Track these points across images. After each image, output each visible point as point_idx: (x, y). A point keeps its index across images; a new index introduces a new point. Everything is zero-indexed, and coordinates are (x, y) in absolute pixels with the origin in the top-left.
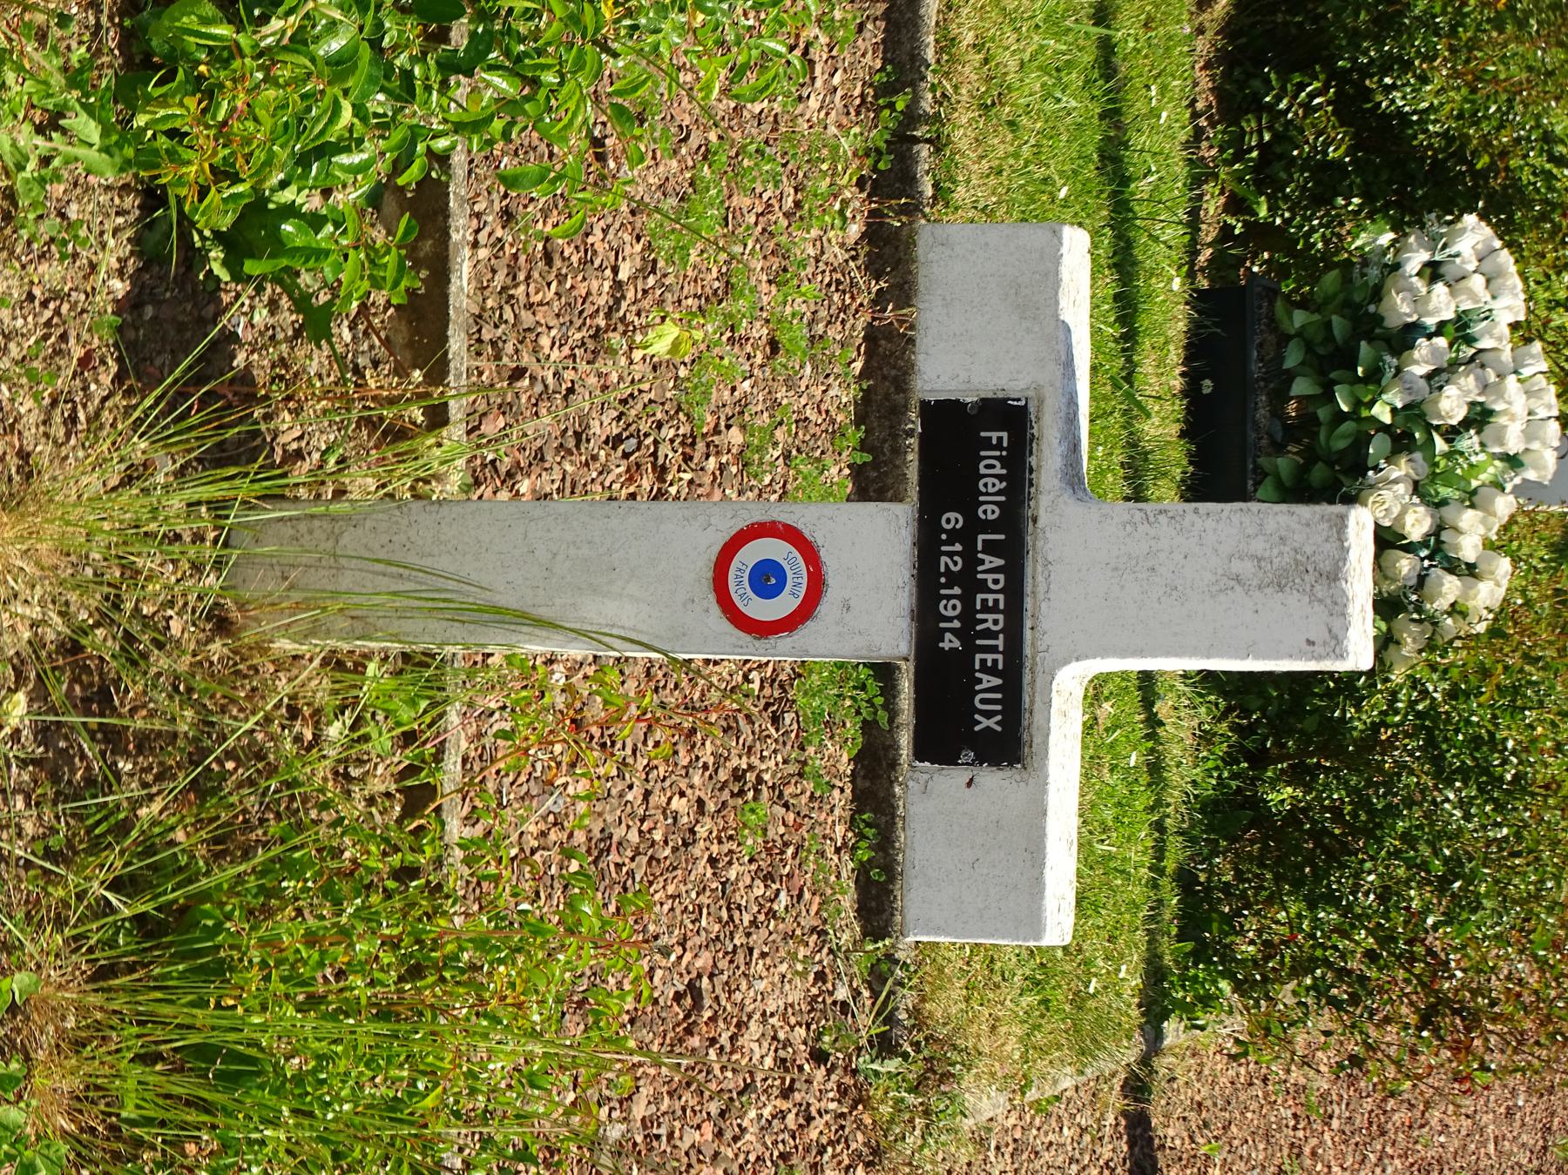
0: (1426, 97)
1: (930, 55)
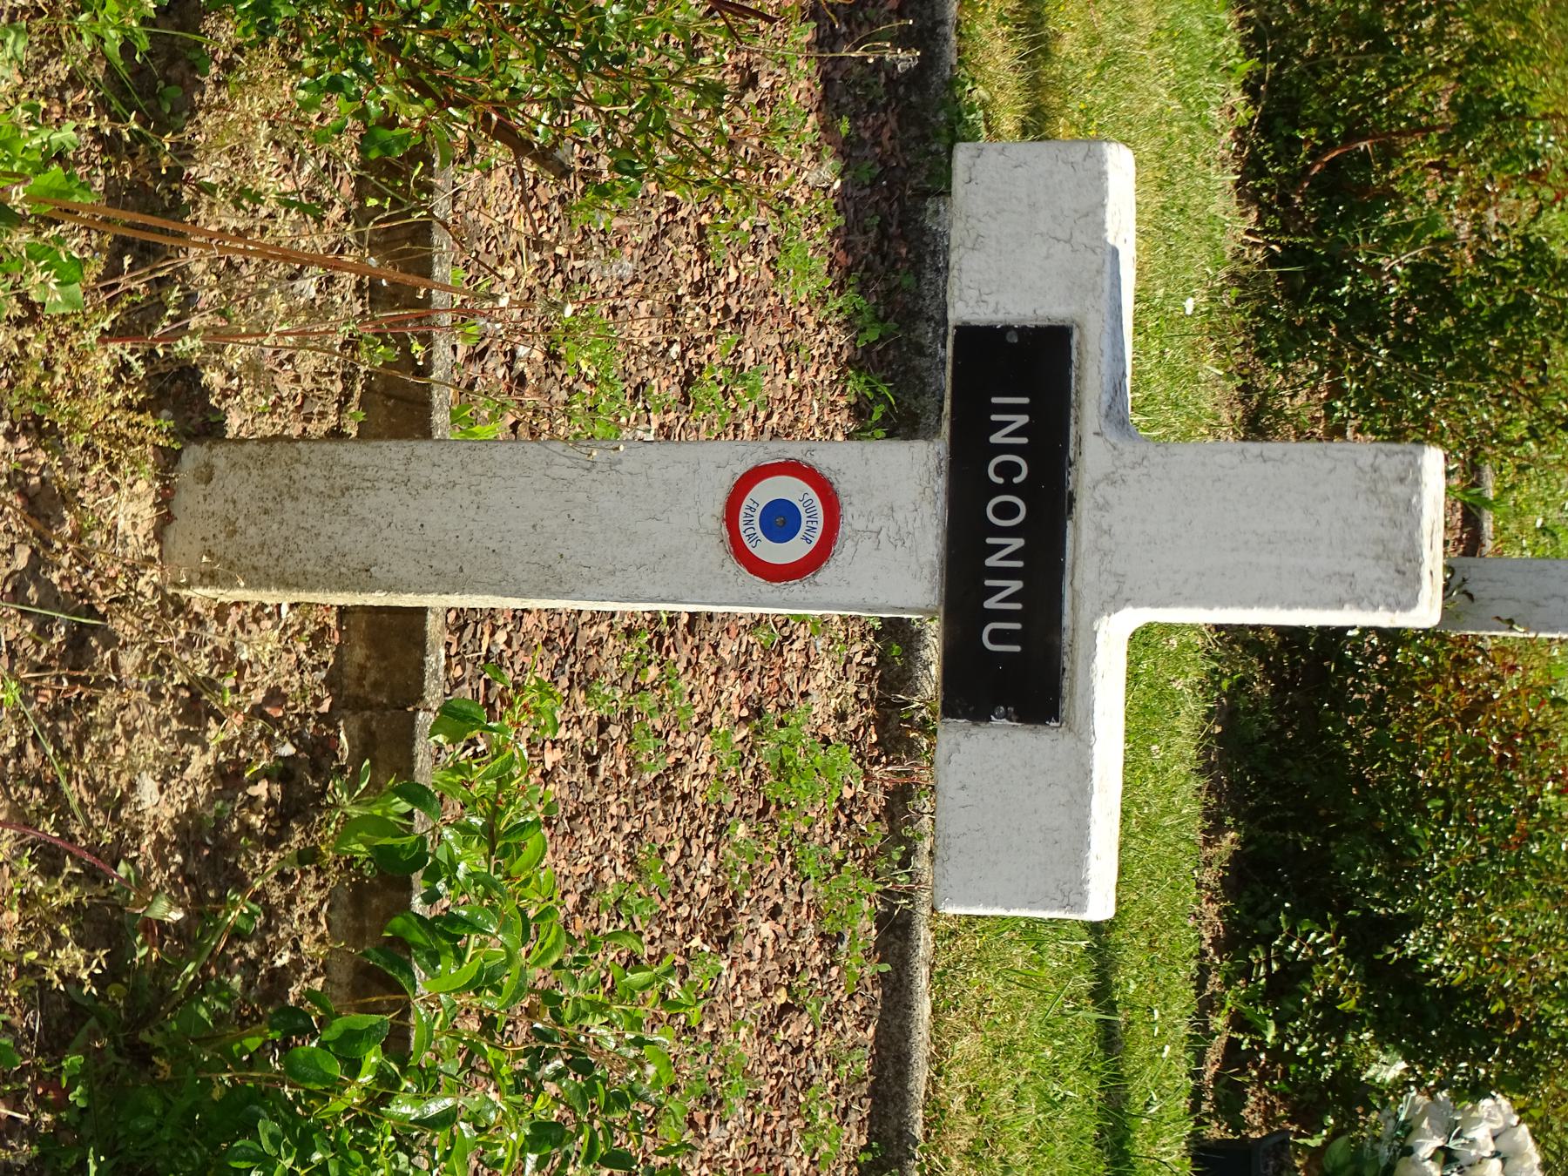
0: (1438, 950)
1: (918, 1131)
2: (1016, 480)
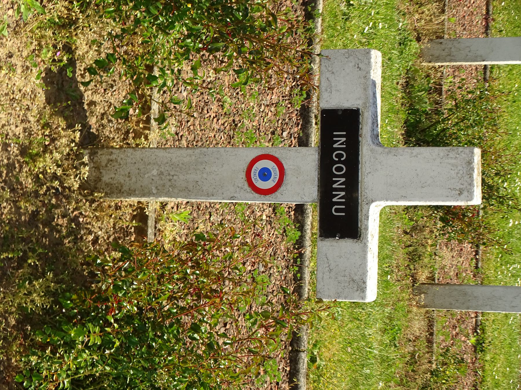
2: (342, 159)
